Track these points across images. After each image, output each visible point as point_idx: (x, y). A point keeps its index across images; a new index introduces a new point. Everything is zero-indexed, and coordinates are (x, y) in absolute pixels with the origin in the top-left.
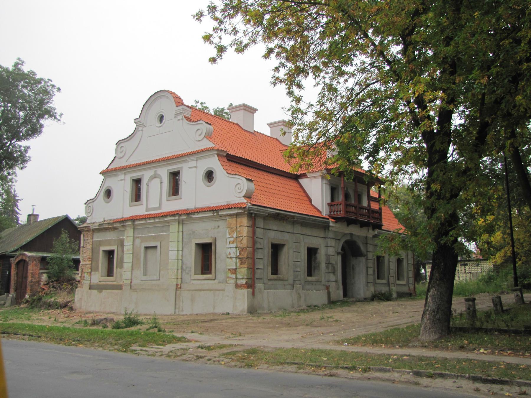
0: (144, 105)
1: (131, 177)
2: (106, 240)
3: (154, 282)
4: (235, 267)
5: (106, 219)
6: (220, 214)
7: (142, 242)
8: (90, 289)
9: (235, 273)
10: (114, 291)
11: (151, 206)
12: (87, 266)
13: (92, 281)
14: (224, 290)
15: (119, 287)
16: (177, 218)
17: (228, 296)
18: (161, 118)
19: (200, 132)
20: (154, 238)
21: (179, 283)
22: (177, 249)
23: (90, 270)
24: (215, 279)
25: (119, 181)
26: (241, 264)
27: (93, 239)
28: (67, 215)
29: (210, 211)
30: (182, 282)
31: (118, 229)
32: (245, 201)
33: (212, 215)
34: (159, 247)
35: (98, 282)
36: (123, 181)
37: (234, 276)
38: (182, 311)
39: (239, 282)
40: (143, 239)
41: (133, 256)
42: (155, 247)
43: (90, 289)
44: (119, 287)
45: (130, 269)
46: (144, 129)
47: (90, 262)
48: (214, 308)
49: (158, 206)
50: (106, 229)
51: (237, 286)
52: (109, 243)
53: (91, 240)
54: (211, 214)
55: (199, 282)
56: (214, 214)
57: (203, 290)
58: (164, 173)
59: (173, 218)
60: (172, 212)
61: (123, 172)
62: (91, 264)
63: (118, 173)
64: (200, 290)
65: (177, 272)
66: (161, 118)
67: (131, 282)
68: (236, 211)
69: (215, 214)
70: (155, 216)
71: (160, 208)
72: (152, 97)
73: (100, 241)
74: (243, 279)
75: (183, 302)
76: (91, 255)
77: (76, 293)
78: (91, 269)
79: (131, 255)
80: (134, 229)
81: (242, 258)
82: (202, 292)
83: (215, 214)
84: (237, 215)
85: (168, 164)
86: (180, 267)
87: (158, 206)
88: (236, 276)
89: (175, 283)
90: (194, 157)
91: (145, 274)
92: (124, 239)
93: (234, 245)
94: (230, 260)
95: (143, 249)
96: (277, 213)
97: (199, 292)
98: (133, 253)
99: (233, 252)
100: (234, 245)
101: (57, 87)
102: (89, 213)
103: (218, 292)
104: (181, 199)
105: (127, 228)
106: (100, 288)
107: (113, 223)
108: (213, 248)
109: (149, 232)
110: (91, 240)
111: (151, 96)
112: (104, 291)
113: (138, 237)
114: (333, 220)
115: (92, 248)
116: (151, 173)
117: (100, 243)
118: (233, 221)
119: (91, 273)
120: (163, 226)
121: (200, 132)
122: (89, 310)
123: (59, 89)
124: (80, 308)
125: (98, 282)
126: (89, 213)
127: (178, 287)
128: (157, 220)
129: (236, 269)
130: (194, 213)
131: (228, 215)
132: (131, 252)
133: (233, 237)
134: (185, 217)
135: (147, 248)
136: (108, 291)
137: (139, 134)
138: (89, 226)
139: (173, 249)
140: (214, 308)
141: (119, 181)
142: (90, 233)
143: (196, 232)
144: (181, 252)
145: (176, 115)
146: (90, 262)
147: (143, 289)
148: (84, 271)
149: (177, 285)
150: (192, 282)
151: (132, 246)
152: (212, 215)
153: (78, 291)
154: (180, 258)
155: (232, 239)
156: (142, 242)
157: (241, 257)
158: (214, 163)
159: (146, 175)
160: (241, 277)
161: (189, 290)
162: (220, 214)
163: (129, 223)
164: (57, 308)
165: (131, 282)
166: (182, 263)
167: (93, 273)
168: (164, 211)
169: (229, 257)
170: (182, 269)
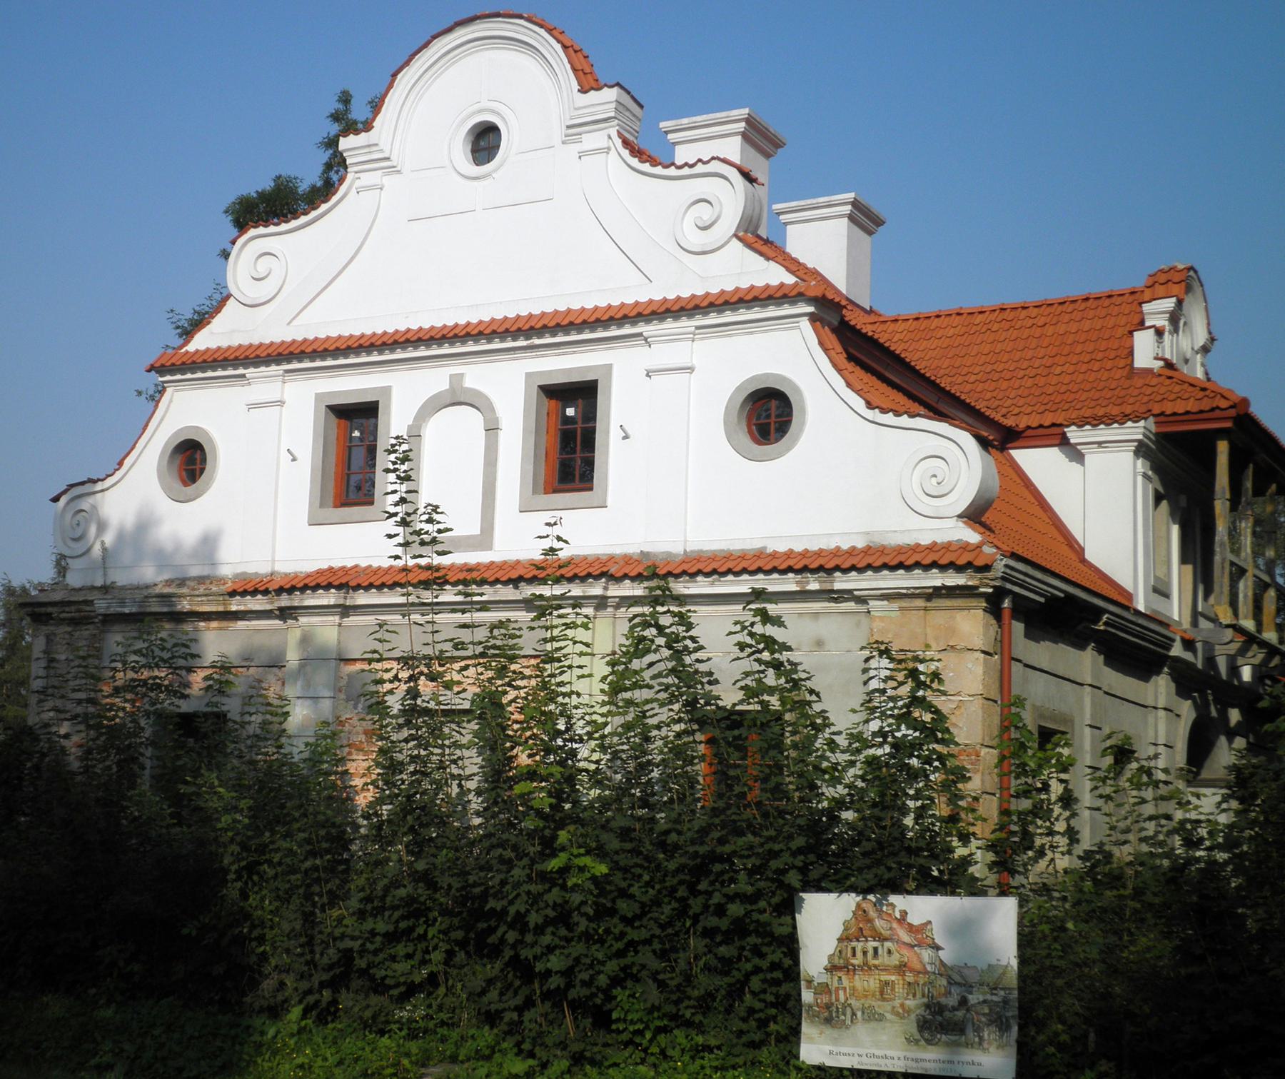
1: (528, 375)
18: (485, 141)
19: (705, 213)
25: (252, 407)
49: (475, 530)
58: (509, 382)
66: (485, 141)
68: (936, 579)
70: (520, 572)
71: (485, 538)
87: (475, 530)
90: (685, 324)
96: (1069, 597)
114: (447, 654)
116: (431, 379)
120: (816, 615)
121: (705, 213)
141: (252, 407)
145: (575, 129)
158: (793, 353)
159: (403, 391)
168: (512, 556)
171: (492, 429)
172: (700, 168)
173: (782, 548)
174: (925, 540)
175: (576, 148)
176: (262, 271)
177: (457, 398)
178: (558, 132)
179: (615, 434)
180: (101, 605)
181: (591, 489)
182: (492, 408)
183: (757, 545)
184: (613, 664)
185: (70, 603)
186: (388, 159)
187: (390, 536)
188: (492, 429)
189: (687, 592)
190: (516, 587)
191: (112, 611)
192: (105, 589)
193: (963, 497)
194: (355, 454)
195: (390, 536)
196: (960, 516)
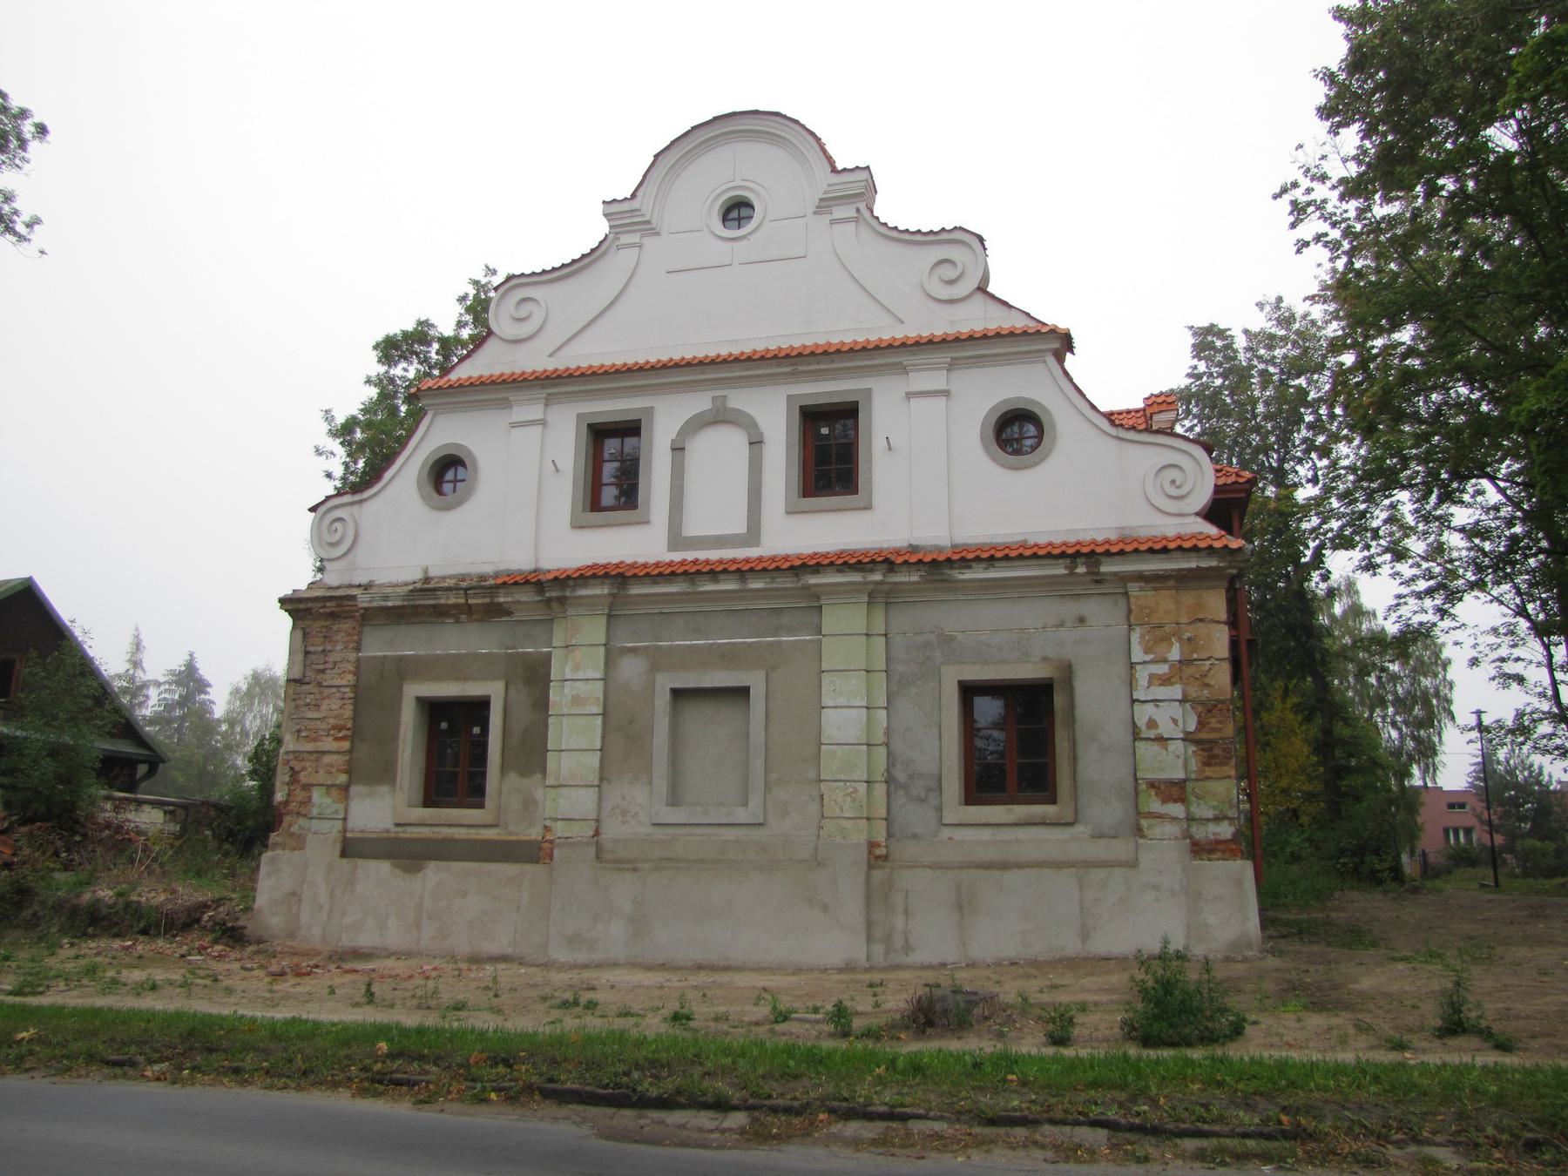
0: (656, 156)
2: (438, 658)
3: (731, 834)
4: (1182, 775)
5: (432, 573)
6: (1103, 569)
7: (655, 668)
8: (344, 854)
9: (1182, 800)
10: (493, 866)
11: (695, 526)
12: (327, 759)
13: (350, 825)
14: (1133, 864)
15: (534, 853)
16: (877, 577)
17: (1155, 888)
18: (737, 210)
19: (948, 272)
20: (729, 657)
21: (880, 835)
22: (858, 706)
23: (342, 778)
24: (1071, 824)
25: (515, 425)
26: (1207, 764)
27: (358, 649)
28: (30, 579)
29: (1056, 557)
30: (889, 835)
31: (509, 613)
32: (1212, 530)
33: (1063, 571)
34: (757, 694)
35: (388, 824)
36: (539, 429)
37: (1177, 810)
38: (907, 948)
39: (1200, 832)
40: (658, 660)
41: (604, 723)
42: (743, 693)
43: (344, 854)
44: (534, 853)
45: (593, 778)
46: (647, 241)
47: (346, 745)
48: (1085, 936)
50: (439, 613)
51: (1200, 849)
52: (455, 667)
53: (352, 656)
54: (1060, 570)
55: (986, 834)
56: (1072, 568)
57: (1020, 866)
58: (773, 412)
59: (856, 577)
60: (852, 554)
61: (543, 393)
62: (351, 751)
63: (513, 396)
64: (1004, 866)
65: (869, 792)
66: (737, 210)
67: (597, 833)
68: (1192, 564)
69: (1081, 569)
71: (753, 534)
72: (695, 134)
73: (401, 658)
74: (1217, 819)
75: (906, 912)
76: (348, 713)
77: (264, 869)
78: (348, 772)
79: (599, 720)
80: (609, 616)
81: (1213, 742)
82: (1010, 877)
83: (1081, 569)
84: (1183, 579)
85: (793, 374)
86: (880, 775)
88: (1187, 810)
89: (861, 838)
90: (944, 357)
91: (674, 800)
92: (549, 656)
93: (1176, 691)
94: (1155, 748)
95: (663, 700)
97: (997, 874)
98: (604, 714)
99: (1170, 715)
100: (1176, 691)
101: (37, 120)
102: (333, 545)
103: (1100, 874)
104: (868, 507)
105: (571, 611)
106: (406, 853)
107: (497, 587)
108: (1059, 700)
109: (698, 632)
110: (352, 656)
111: (693, 128)
112: (432, 866)
113: (634, 650)
115: (355, 687)
116: (700, 402)
117: (404, 669)
118: (1164, 603)
119: (345, 789)
121: (948, 272)
122: (347, 941)
123: (42, 130)
124: (292, 935)
125: (388, 824)
126: (333, 545)
127: (876, 857)
128: (756, 584)
129: (1185, 781)
130: (965, 563)
131: (1141, 577)
132: (598, 709)
133: (1165, 661)
134: (915, 578)
135: (678, 694)
136: (457, 866)
137: (620, 262)
138: (354, 597)
139: (842, 701)
140: (1085, 936)
142: (347, 625)
143: (959, 636)
144: (882, 715)
146: (346, 745)
147: (670, 859)
148: (303, 778)
149: (872, 845)
150: (947, 832)
151: (600, 685)
152: (1063, 571)
153: (273, 861)
154: (880, 737)
155: (1162, 669)
156: (655, 668)
157: (1204, 736)
160: (1210, 814)
161: (936, 866)
162: (1103, 569)
163: (600, 590)
164: (144, 932)
165: (597, 833)
166: (889, 754)
167: (354, 790)
169: (1152, 734)
170: (889, 780)
171: (756, 443)
172: (944, 236)
173: (1042, 540)
174: (1171, 533)
175: (826, 219)
176: (523, 313)
177: (721, 417)
178: (811, 208)
179: (878, 445)
180: (364, 600)
181: (856, 492)
182: (755, 425)
183: (1019, 538)
184: (1444, 1088)
185: (331, 598)
186: (648, 222)
187: (319, 452)
188: (756, 443)
189: (961, 577)
190: (796, 575)
191: (375, 604)
192: (366, 587)
193: (1203, 495)
194: (613, 470)
195: (319, 452)
196: (1197, 514)
